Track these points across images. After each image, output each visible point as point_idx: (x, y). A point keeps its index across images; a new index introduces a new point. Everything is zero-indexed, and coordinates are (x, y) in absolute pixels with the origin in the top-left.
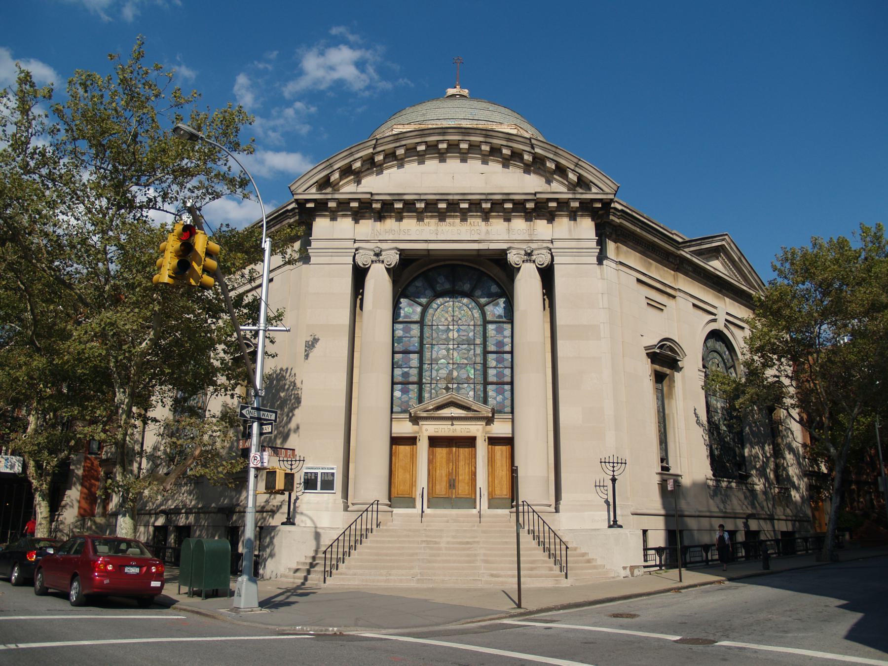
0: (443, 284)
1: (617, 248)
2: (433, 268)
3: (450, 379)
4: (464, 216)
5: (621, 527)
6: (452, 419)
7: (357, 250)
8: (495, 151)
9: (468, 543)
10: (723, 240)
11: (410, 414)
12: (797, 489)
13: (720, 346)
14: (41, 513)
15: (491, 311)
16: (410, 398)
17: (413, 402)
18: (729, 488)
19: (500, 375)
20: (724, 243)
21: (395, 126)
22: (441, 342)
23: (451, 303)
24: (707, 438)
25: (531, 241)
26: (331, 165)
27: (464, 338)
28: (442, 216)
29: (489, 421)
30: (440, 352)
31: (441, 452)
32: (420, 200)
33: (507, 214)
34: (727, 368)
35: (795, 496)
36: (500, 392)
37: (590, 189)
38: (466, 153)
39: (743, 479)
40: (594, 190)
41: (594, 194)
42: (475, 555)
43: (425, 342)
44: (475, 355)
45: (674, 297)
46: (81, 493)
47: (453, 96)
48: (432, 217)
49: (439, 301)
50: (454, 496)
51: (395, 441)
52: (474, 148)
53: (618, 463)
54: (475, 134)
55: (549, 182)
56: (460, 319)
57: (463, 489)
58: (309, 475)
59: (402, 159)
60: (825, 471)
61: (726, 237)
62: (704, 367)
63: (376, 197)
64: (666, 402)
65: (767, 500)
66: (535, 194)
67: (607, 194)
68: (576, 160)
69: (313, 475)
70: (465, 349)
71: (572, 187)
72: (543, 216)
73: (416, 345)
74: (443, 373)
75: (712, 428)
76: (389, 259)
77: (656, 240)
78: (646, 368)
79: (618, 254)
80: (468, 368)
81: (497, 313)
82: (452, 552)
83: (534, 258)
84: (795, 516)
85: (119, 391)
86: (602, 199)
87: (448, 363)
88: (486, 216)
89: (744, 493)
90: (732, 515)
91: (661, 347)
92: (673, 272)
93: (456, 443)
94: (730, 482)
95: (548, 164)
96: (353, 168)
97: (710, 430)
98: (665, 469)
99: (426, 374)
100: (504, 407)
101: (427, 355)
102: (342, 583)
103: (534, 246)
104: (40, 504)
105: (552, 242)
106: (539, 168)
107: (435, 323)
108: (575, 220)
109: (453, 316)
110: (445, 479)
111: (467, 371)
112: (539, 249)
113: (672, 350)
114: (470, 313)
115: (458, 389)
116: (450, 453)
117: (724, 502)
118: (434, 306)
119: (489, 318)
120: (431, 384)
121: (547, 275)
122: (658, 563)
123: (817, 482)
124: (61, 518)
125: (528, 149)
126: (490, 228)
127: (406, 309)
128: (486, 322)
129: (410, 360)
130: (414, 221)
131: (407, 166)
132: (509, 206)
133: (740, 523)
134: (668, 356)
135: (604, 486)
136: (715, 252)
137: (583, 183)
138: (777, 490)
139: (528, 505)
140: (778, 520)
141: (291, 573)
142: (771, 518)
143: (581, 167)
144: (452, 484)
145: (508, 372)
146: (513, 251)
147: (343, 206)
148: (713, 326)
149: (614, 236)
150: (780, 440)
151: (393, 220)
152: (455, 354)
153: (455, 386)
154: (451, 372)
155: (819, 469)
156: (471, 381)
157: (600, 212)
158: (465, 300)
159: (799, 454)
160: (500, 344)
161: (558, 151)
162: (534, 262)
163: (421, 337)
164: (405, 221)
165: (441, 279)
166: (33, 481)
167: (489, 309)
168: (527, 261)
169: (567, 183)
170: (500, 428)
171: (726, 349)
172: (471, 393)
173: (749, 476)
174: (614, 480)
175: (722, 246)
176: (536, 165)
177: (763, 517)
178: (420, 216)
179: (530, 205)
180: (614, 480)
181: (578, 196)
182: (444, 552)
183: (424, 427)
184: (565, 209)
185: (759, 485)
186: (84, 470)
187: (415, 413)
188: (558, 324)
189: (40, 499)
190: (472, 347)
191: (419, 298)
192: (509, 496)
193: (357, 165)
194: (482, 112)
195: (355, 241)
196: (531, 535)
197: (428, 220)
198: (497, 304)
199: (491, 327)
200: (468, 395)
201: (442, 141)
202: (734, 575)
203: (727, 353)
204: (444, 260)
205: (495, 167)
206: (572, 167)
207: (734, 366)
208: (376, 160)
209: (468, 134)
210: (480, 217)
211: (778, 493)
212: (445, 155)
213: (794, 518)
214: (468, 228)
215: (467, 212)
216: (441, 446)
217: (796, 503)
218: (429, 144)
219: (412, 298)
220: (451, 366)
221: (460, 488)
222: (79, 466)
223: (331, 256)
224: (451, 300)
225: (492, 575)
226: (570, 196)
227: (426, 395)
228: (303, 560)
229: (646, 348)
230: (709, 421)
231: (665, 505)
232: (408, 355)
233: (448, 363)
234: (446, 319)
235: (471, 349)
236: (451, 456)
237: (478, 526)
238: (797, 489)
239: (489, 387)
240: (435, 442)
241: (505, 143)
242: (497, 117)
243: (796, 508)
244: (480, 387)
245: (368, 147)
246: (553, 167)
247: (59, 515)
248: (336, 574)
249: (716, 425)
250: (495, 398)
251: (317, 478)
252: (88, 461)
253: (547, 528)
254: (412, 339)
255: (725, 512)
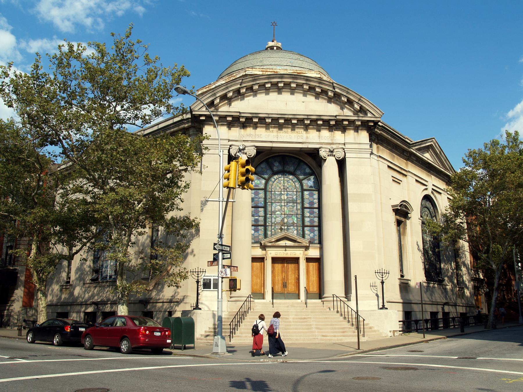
0: (277, 166)
1: (378, 147)
2: (272, 157)
3: (283, 223)
4: (294, 127)
5: (387, 309)
6: (286, 247)
7: (230, 146)
8: (312, 89)
9: (305, 318)
10: (432, 141)
11: (261, 244)
12: (468, 288)
13: (428, 204)
14: (42, 304)
15: (306, 184)
16: (259, 235)
17: (261, 237)
18: (434, 287)
19: (312, 221)
20: (432, 143)
21: (247, 69)
22: (277, 202)
23: (283, 178)
24: (423, 258)
25: (332, 144)
26: (215, 94)
27: (291, 199)
28: (280, 127)
29: (307, 248)
30: (276, 207)
31: (278, 266)
32: (269, 118)
33: (319, 127)
34: (432, 217)
35: (467, 293)
36: (312, 231)
37: (366, 114)
38: (294, 89)
39: (441, 282)
40: (369, 115)
41: (369, 117)
42: (311, 325)
43: (267, 201)
44: (297, 209)
45: (406, 176)
46: (24, 292)
47: (272, 48)
48: (274, 127)
49: (276, 177)
50: (286, 292)
51: (255, 260)
52: (300, 86)
53: (200, 272)
54: (300, 79)
55: (342, 109)
56: (288, 188)
57: (291, 288)
58: (206, 280)
59: (256, 91)
60: (482, 278)
61: (434, 140)
62: (421, 217)
63: (243, 115)
64: (402, 237)
65: (453, 294)
66: (336, 116)
67: (377, 117)
68: (359, 97)
69: (208, 280)
70: (291, 206)
71: (356, 112)
72: (339, 129)
73: (262, 203)
74: (279, 220)
75: (425, 252)
76: (250, 152)
77: (398, 143)
78: (392, 218)
79: (378, 151)
80: (293, 217)
81: (310, 185)
82: (297, 324)
83: (334, 153)
84: (467, 304)
85: (115, 233)
86: (374, 121)
87: (282, 214)
88: (306, 128)
89: (442, 291)
90: (436, 303)
91: (400, 206)
92: (405, 161)
93: (287, 261)
94: (434, 284)
95: (343, 99)
96: (228, 96)
97: (424, 254)
98: (402, 276)
99: (269, 220)
100: (314, 240)
101: (269, 209)
102: (240, 341)
103: (334, 146)
104: (41, 299)
105: (345, 145)
106: (337, 100)
107: (273, 190)
108: (358, 132)
109: (284, 186)
110: (280, 282)
111: (293, 219)
112: (337, 148)
113: (406, 207)
114: (294, 184)
115: (288, 229)
116: (283, 267)
117: (431, 295)
118: (273, 180)
119: (305, 187)
120: (271, 226)
121: (341, 164)
122: (415, 328)
123: (478, 283)
124: (11, 308)
125: (331, 89)
126: (308, 135)
127: (256, 181)
128: (303, 190)
129: (259, 212)
130: (263, 130)
131: (259, 96)
132: (320, 122)
133: (440, 308)
134: (404, 211)
135: (375, 286)
136: (427, 149)
137: (363, 110)
138: (457, 289)
139: (337, 297)
140: (459, 306)
141: (203, 337)
142: (455, 305)
143: (362, 101)
144: (285, 285)
145: (316, 220)
146: (323, 149)
147: (222, 119)
148: (426, 193)
149: (376, 140)
150: (459, 260)
151: (251, 129)
152: (286, 209)
153: (286, 227)
154: (283, 219)
155: (479, 276)
156: (295, 225)
157: (372, 128)
158: (291, 177)
159: (469, 268)
160: (312, 203)
161: (349, 91)
162: (334, 156)
163: (265, 199)
164: (258, 129)
165: (276, 164)
166: (36, 285)
167: (305, 182)
168: (330, 155)
169: (353, 110)
170: (314, 253)
171: (431, 206)
172: (295, 232)
173: (443, 280)
174: (383, 283)
175: (431, 145)
176: (336, 98)
177: (451, 304)
178: (267, 126)
179: (332, 123)
180: (383, 283)
181: (361, 118)
182: (292, 323)
183: (269, 252)
184: (352, 125)
185: (449, 287)
186: (26, 277)
187: (264, 243)
188: (349, 192)
189: (41, 295)
190: (295, 204)
191: (263, 175)
192: (317, 292)
193: (230, 94)
194: (296, 61)
195: (229, 140)
196: (339, 314)
197: (272, 129)
198: (309, 180)
199: (306, 193)
200: (293, 233)
201: (281, 82)
202: (450, 335)
203: (432, 208)
204: (279, 153)
205: (310, 98)
206: (357, 101)
207: (435, 216)
208: (241, 92)
209: (296, 78)
210: (303, 128)
211: (459, 290)
212: (281, 90)
213: (467, 305)
214: (296, 135)
215: (295, 125)
216: (278, 263)
217: (467, 297)
218: (272, 83)
219: (260, 175)
220: (283, 216)
221: (290, 287)
222: (22, 275)
223: (215, 149)
224: (283, 176)
225: (323, 336)
226: (356, 118)
227: (269, 233)
228: (208, 330)
229: (393, 206)
230: (423, 249)
231: (402, 298)
232: (258, 209)
233: (282, 214)
234: (280, 188)
235: (295, 206)
236: (284, 269)
237: (306, 309)
238: (468, 288)
239: (306, 228)
240: (275, 260)
241: (317, 85)
242: (305, 65)
243: (467, 300)
244: (300, 228)
245: (237, 84)
246: (346, 100)
247: (10, 306)
248: (235, 337)
249: (427, 250)
250: (309, 235)
251: (210, 282)
252: (28, 271)
253: (350, 310)
254: (260, 199)
255: (432, 301)
